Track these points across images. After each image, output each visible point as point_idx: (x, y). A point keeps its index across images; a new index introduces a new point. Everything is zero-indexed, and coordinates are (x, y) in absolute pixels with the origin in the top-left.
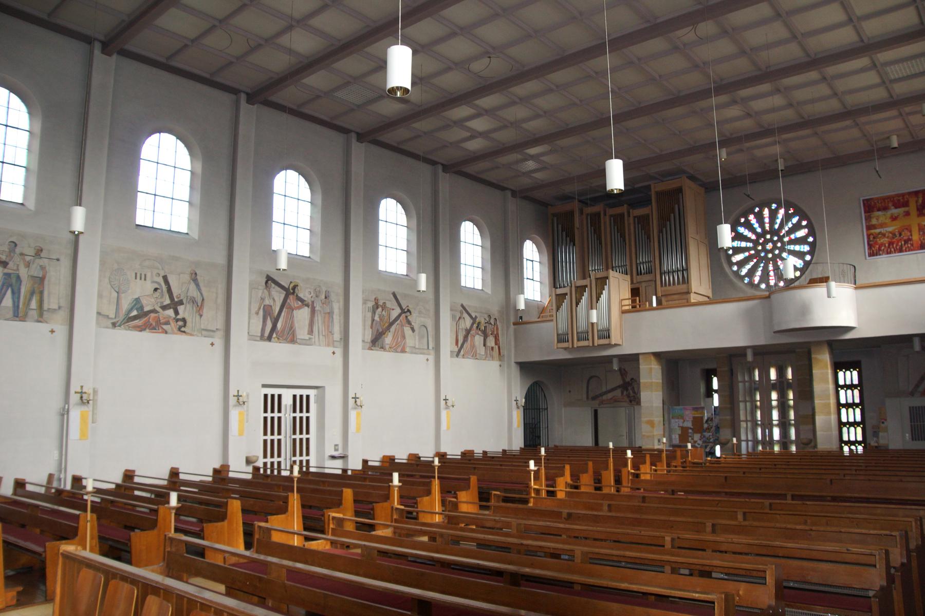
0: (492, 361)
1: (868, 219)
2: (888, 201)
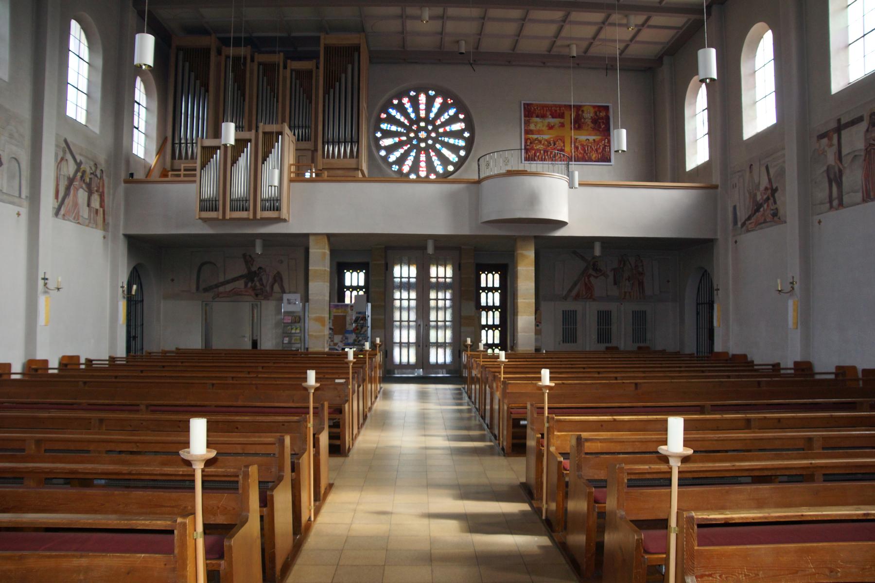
0: (94, 230)
1: (527, 123)
2: (546, 110)
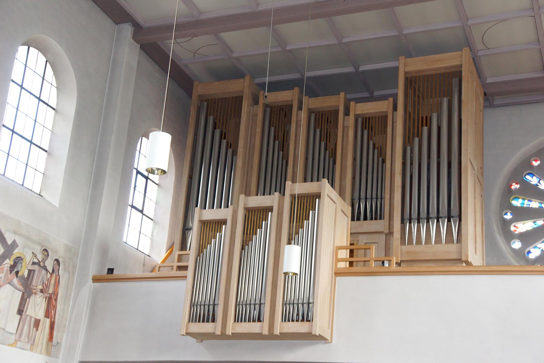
0: (29, 353)
